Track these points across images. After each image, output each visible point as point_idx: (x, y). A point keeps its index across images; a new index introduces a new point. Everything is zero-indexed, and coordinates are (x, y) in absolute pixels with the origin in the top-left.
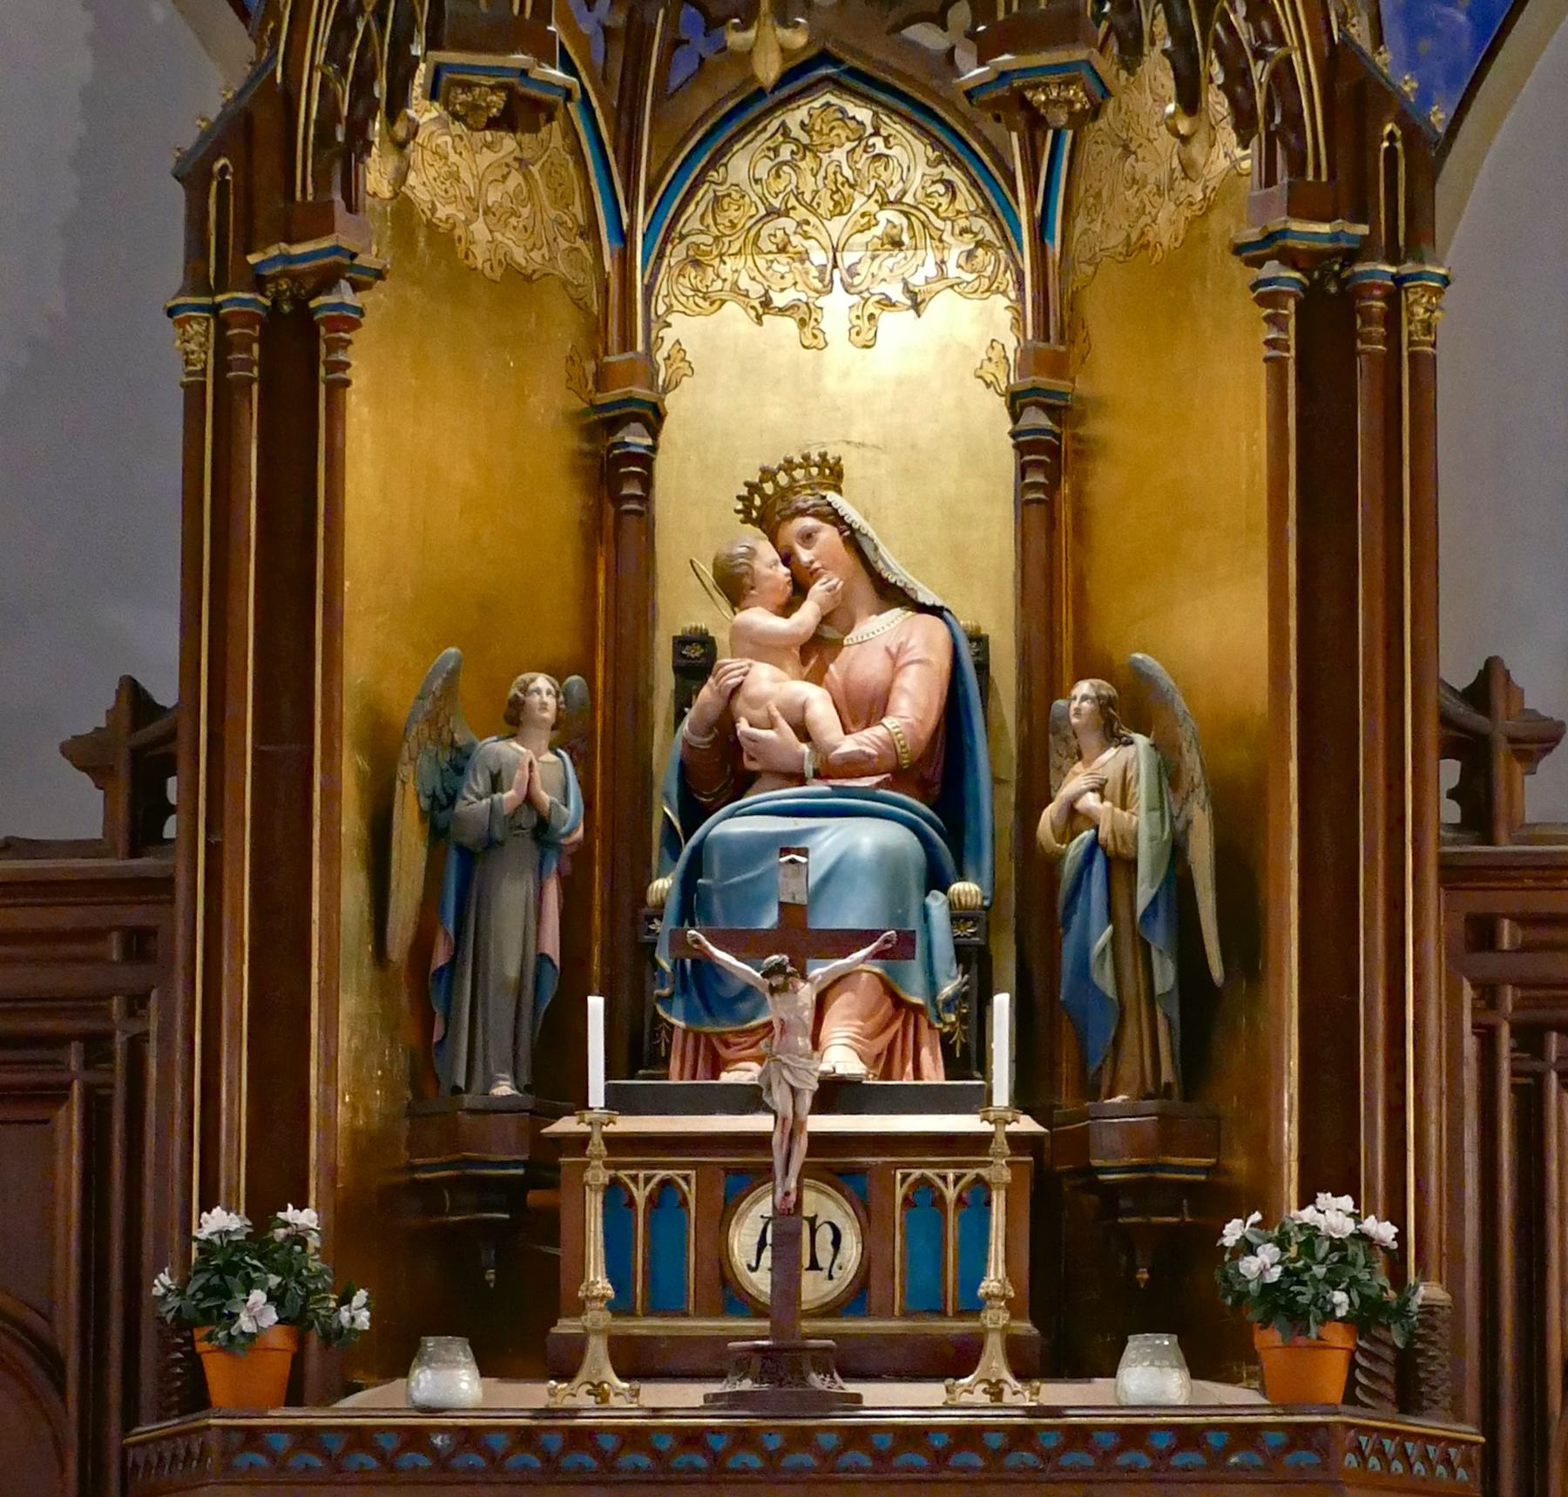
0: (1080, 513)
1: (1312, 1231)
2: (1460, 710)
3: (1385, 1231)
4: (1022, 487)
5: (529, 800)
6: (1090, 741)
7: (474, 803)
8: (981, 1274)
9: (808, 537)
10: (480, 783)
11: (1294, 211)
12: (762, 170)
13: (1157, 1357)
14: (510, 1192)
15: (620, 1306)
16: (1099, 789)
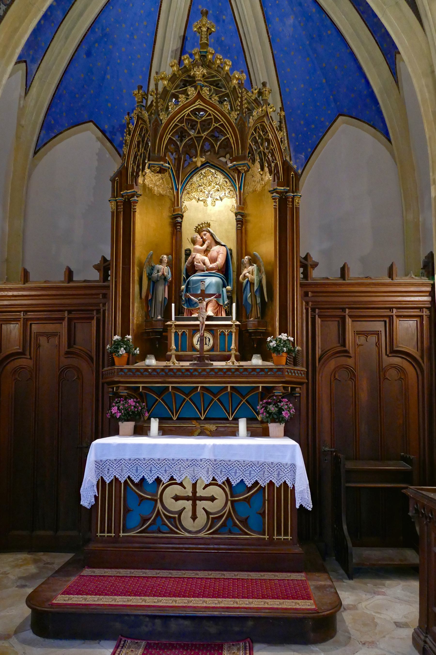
0: (246, 231)
1: (281, 339)
3: (292, 339)
4: (237, 227)
5: (163, 274)
7: (155, 275)
10: (156, 272)
12: (198, 179)
13: (257, 358)
14: (160, 333)
15: (177, 350)
16: (249, 272)
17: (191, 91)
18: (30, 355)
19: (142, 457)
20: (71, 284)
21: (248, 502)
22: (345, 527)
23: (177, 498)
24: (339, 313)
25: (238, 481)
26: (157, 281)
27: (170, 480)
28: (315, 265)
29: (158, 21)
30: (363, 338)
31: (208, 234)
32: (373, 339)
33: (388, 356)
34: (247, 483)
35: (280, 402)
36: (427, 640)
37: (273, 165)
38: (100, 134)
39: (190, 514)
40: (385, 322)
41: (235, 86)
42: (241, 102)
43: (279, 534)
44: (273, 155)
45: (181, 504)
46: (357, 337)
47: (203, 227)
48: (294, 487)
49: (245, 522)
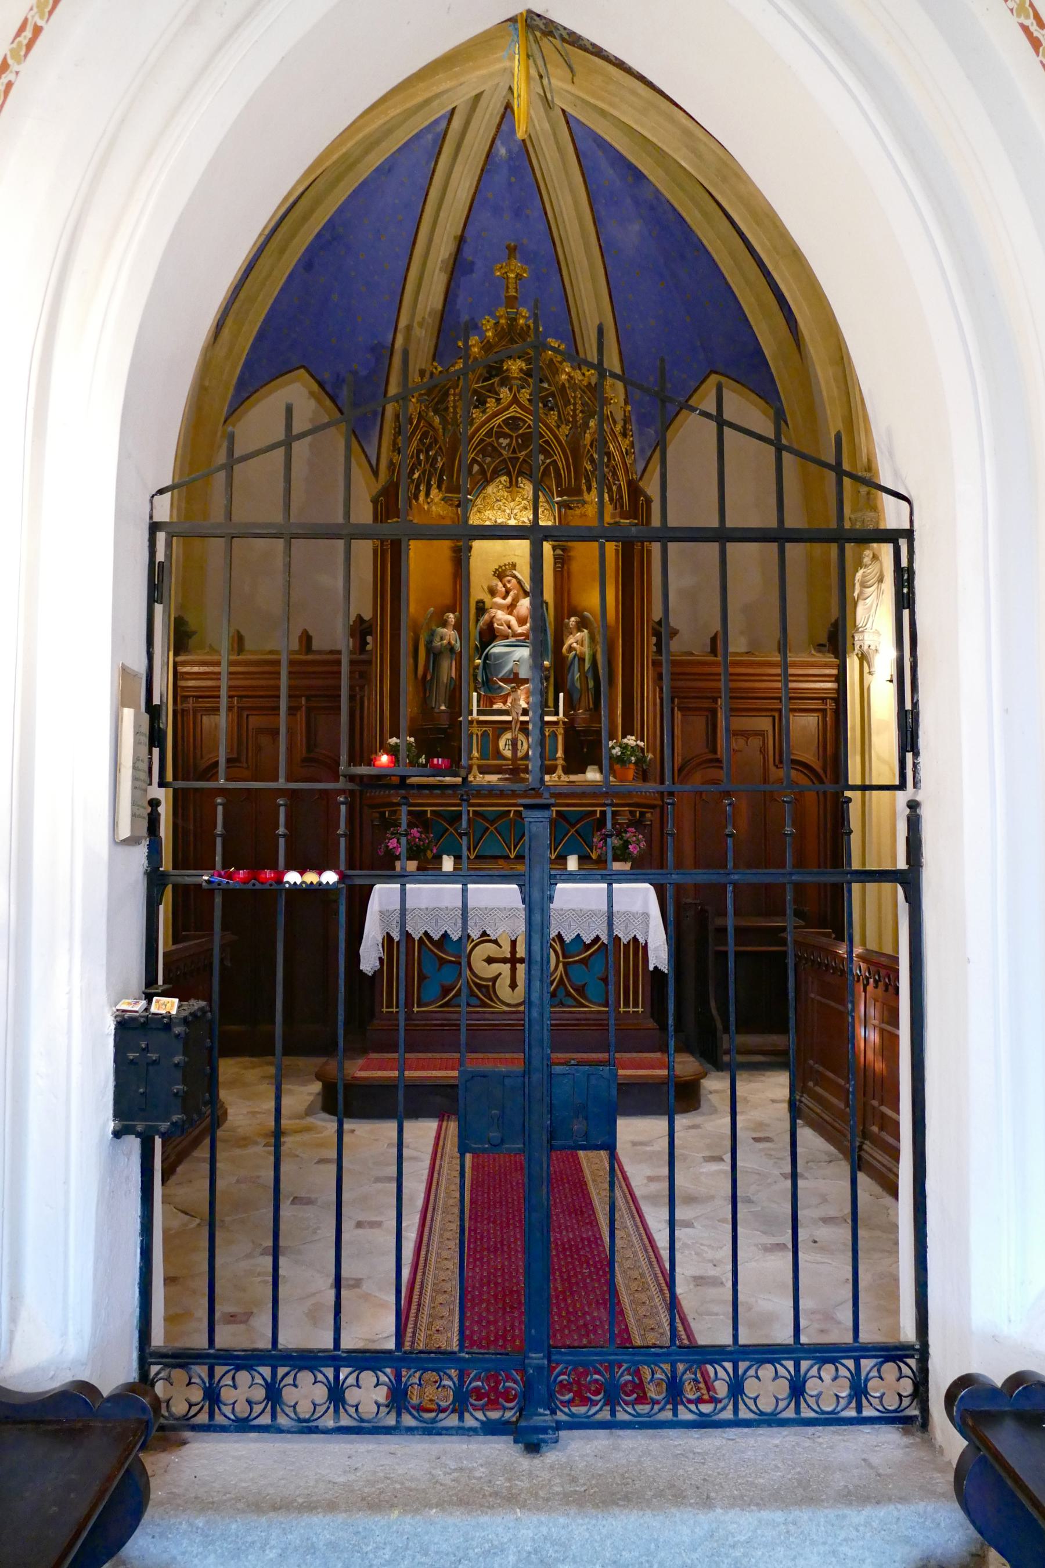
0: (569, 573)
1: (627, 744)
2: (657, 627)
3: (642, 744)
4: (555, 568)
5: (449, 643)
6: (575, 631)
7: (437, 643)
8: (557, 752)
9: (509, 581)
10: (438, 639)
11: (622, 518)
12: (495, 490)
13: (594, 771)
14: (443, 731)
15: (482, 758)
16: (576, 642)
17: (505, 393)
18: (247, 762)
19: (443, 905)
20: (310, 657)
21: (586, 965)
22: (713, 1004)
23: (490, 960)
24: (706, 704)
25: (574, 936)
26: (441, 653)
27: (482, 936)
28: (674, 633)
29: (421, 215)
30: (741, 741)
31: (514, 581)
32: (756, 742)
33: (777, 767)
34: (585, 939)
35: (626, 832)
36: (803, 1099)
37: (614, 488)
38: (315, 387)
39: (508, 982)
40: (774, 717)
41: (563, 384)
42: (574, 410)
43: (627, 1005)
44: (615, 474)
45: (497, 967)
46: (733, 740)
47: (505, 570)
48: (646, 943)
49: (581, 990)
